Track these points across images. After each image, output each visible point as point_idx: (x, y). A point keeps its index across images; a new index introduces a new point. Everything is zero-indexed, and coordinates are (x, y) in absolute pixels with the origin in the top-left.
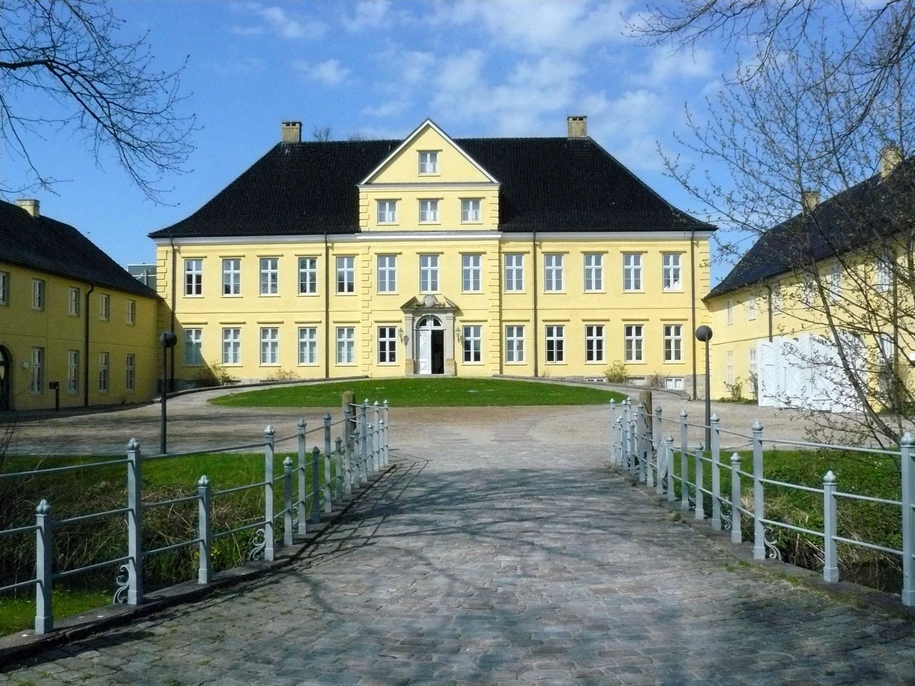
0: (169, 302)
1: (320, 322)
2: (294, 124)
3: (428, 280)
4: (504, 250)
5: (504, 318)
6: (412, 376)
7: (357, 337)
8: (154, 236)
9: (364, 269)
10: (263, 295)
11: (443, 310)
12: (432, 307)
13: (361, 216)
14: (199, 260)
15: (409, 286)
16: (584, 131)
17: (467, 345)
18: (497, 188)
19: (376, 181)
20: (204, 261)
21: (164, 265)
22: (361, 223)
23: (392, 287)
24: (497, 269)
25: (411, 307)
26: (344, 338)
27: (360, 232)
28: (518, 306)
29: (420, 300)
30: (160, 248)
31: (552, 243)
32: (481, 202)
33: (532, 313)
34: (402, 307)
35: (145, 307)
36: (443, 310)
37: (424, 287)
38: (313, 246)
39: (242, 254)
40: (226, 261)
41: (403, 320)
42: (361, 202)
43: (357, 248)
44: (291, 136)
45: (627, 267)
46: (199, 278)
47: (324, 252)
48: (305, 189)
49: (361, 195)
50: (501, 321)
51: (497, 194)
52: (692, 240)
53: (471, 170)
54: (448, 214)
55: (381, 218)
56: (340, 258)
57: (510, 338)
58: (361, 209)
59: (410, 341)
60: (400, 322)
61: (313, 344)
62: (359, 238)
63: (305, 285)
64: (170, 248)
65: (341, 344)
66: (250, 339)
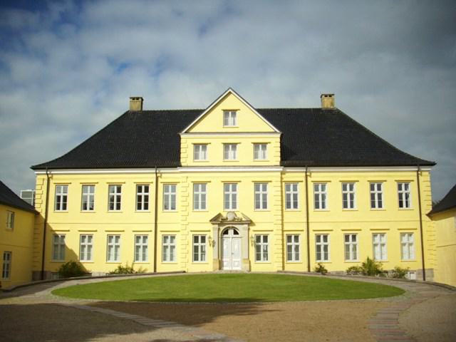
0: (43, 215)
1: (302, 231)
2: (138, 99)
3: (230, 201)
4: (284, 180)
5: (285, 229)
6: (218, 271)
7: (177, 242)
8: (35, 168)
9: (184, 194)
10: (195, 210)
11: (241, 222)
12: (233, 221)
13: (182, 155)
14: (66, 185)
15: (215, 205)
16: (332, 104)
17: (258, 248)
18: (279, 136)
19: (192, 131)
20: (208, 185)
21: (40, 190)
22: (182, 160)
23: (204, 207)
24: (280, 193)
25: (218, 220)
26: (168, 243)
27: (181, 166)
28: (295, 220)
29: (224, 215)
30: (39, 177)
31: (319, 175)
32: (268, 146)
33: (305, 225)
34: (211, 221)
35: (23, 219)
36: (241, 222)
37: (227, 206)
38: (145, 176)
39: (356, 179)
40: (85, 186)
41: (211, 229)
42: (182, 146)
43: (178, 178)
44: (136, 107)
45: (227, 193)
46: (65, 198)
47: (154, 181)
48: (146, 140)
49: (182, 141)
50: (283, 231)
51: (279, 140)
52: (418, 171)
53: (266, 126)
54: (244, 153)
55: (196, 157)
56: (166, 186)
57: (289, 244)
58: (182, 150)
59: (216, 245)
60: (209, 231)
61: (145, 247)
62: (288, 170)
63: (142, 203)
64: (46, 177)
65: (165, 247)
66: (99, 243)
